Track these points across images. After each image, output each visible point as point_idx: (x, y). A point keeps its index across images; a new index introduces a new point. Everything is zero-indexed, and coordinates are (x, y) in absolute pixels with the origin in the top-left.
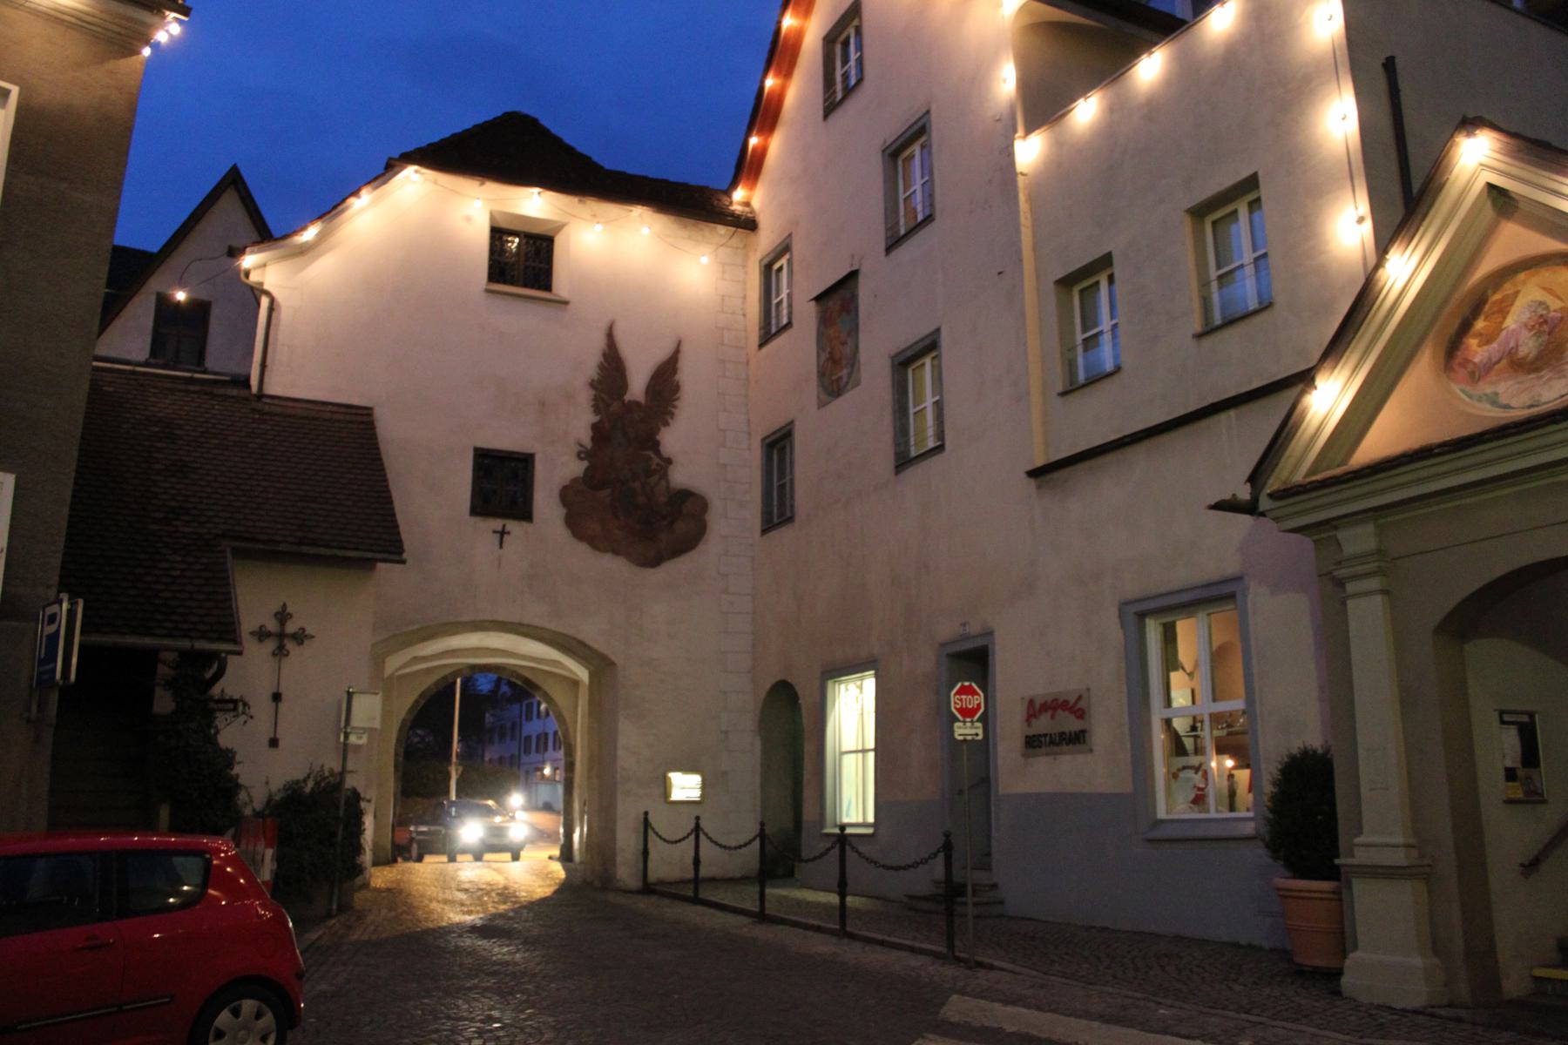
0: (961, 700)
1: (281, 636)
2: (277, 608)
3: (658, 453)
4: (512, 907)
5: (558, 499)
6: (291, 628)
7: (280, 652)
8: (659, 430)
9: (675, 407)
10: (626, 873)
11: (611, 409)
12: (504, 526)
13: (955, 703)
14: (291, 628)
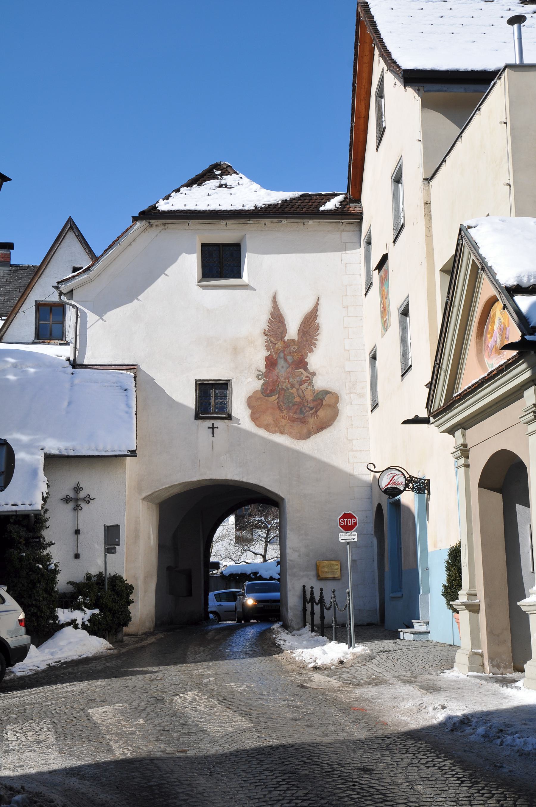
0: (344, 521)
1: (77, 500)
2: (73, 485)
3: (306, 369)
4: (370, 654)
5: (246, 406)
6: (82, 495)
7: (77, 508)
8: (307, 355)
9: (317, 340)
10: (70, 609)
11: (277, 346)
12: (213, 424)
13: (340, 523)
14: (82, 495)
